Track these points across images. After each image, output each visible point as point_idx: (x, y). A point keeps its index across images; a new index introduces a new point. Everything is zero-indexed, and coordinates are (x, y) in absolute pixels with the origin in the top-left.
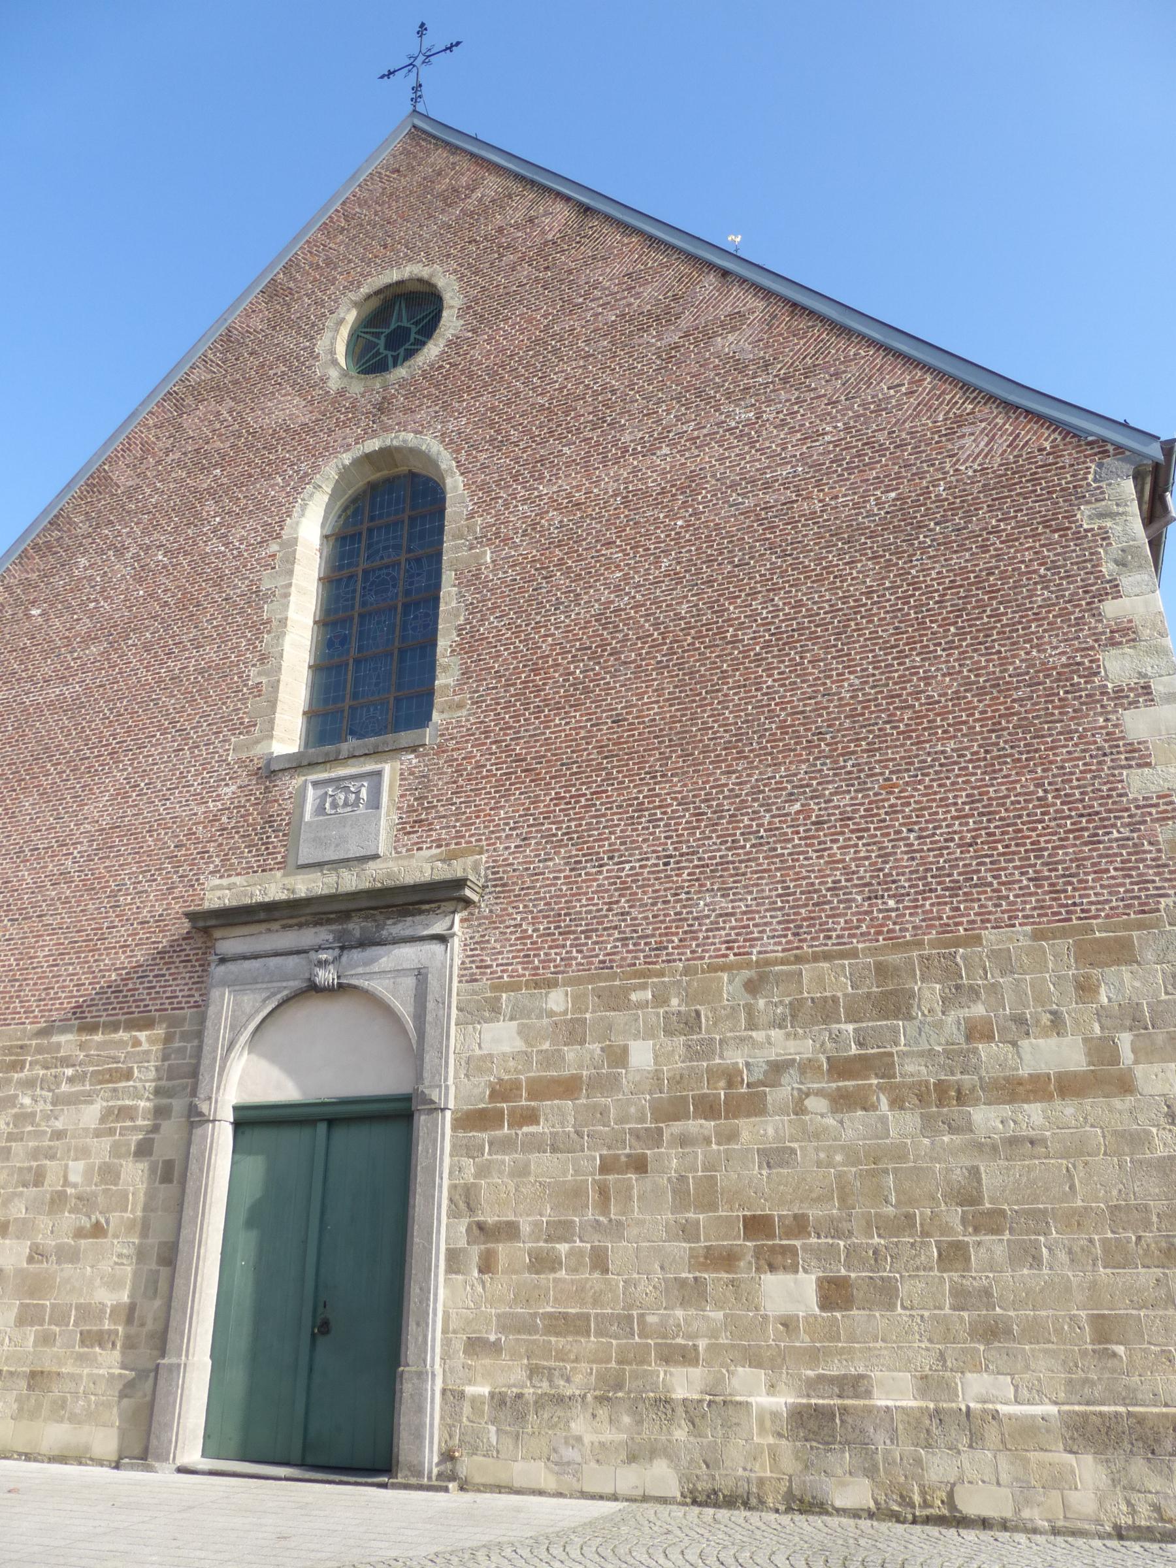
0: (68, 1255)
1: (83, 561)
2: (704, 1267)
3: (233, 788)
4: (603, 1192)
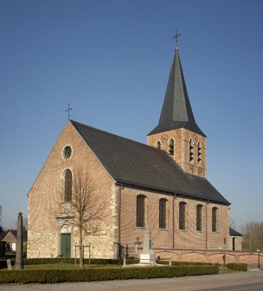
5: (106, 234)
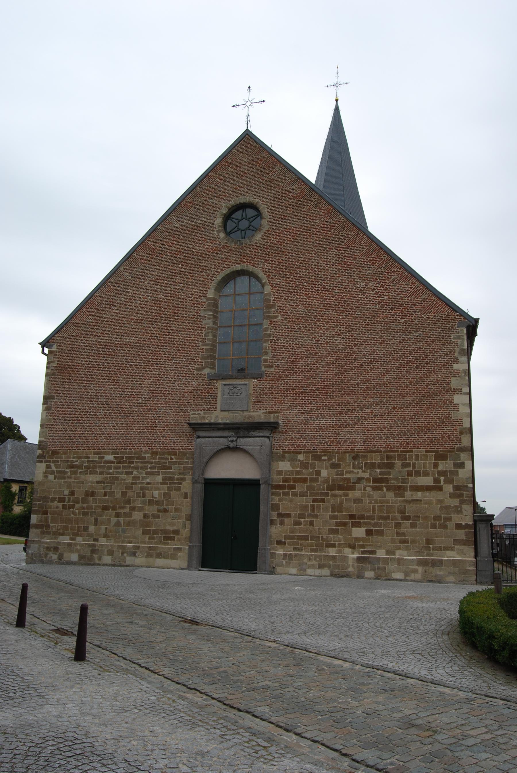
0: (155, 516)
1: (131, 292)
2: (339, 526)
3: (197, 383)
4: (313, 506)
5: (437, 487)
